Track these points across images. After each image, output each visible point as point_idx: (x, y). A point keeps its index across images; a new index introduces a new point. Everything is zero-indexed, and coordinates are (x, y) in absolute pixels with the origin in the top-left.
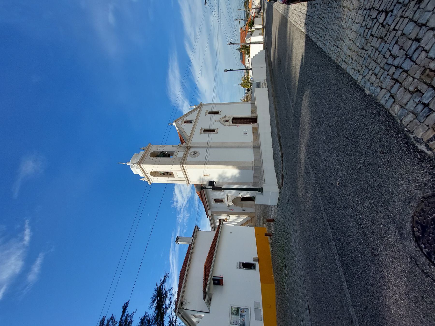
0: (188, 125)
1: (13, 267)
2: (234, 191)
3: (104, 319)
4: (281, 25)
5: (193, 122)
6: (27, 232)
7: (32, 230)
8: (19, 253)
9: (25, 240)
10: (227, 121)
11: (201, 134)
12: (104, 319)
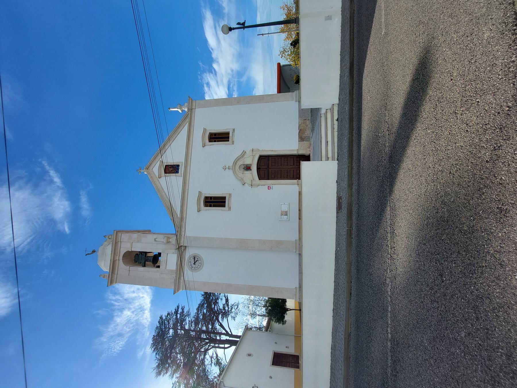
0: (172, 177)
1: (62, 207)
2: (258, 22)
3: (178, 307)
4: (408, 98)
5: (182, 169)
6: (52, 173)
7: (57, 171)
8: (59, 194)
9: (56, 182)
10: (248, 168)
11: (204, 146)
12: (178, 307)
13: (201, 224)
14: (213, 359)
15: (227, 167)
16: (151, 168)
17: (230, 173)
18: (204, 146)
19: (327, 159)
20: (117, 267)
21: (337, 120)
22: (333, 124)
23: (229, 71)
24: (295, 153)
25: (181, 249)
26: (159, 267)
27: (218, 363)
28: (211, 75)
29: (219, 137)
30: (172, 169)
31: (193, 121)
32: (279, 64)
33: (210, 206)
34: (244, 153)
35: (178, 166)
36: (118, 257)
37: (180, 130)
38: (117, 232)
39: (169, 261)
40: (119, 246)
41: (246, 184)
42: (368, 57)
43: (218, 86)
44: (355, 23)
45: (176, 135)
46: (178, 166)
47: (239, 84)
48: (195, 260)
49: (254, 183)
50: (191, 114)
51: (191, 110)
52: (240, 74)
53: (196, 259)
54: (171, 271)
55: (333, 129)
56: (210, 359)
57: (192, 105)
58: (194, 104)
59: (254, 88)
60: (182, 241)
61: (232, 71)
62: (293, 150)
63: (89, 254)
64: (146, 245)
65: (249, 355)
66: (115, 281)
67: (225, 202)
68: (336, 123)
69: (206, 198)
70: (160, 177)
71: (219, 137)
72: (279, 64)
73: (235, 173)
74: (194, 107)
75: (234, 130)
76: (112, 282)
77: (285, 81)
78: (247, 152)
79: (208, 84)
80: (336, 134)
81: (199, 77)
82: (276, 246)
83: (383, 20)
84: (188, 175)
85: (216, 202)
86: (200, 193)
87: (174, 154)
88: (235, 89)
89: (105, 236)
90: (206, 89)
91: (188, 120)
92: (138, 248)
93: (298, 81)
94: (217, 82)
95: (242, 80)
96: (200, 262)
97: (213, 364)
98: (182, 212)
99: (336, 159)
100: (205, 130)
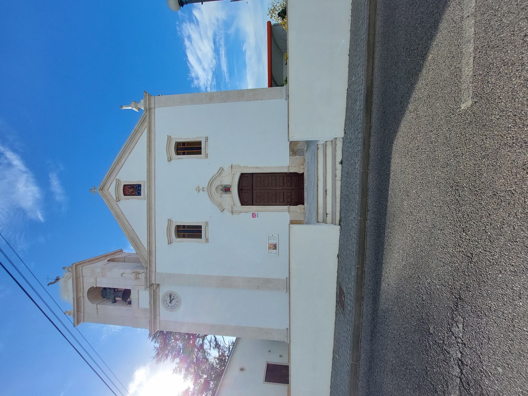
0: (132, 201)
5: (144, 190)
10: (227, 189)
11: (170, 160)
13: (174, 257)
14: (211, 343)
15: (201, 188)
16: (106, 188)
17: (204, 195)
18: (170, 160)
19: (325, 222)
20: (82, 305)
21: (341, 163)
22: (334, 169)
23: (214, 21)
24: (285, 171)
25: (153, 287)
26: (130, 303)
27: (217, 346)
28: (193, 26)
29: (189, 148)
30: (132, 190)
31: (153, 126)
32: (269, 23)
33: (184, 237)
34: (221, 170)
35: (140, 186)
36: (81, 293)
37: (137, 137)
38: (76, 266)
39: (141, 297)
40: (82, 280)
41: (225, 211)
42: (408, 117)
43: (202, 40)
44: (378, 12)
45: (133, 144)
46: (140, 186)
47: (227, 37)
48: (171, 297)
49: (235, 209)
50: (150, 116)
51: (149, 110)
52: (227, 24)
53: (172, 297)
54: (145, 310)
55: (334, 176)
56: (208, 344)
57: (149, 104)
58: (152, 101)
59: (244, 42)
60: (153, 279)
61: (218, 20)
62: (283, 167)
63: (51, 283)
64: (114, 277)
65: (242, 370)
66: (82, 319)
67: (201, 232)
68: (339, 167)
69: (178, 227)
70: (118, 200)
71: (189, 148)
72: (269, 23)
73: (211, 196)
74: (153, 106)
75: (207, 139)
76: (78, 322)
77: (277, 45)
78: (225, 169)
79: (189, 37)
80: (338, 184)
81: (178, 28)
82: (265, 284)
83: (468, 71)
84: (153, 197)
85: (190, 232)
86: (170, 221)
87: (132, 170)
88: (222, 43)
89: (64, 268)
90: (187, 43)
91: (146, 124)
92: (104, 283)
93: (286, 81)
94: (200, 35)
95: (230, 32)
96: (176, 300)
97: (212, 348)
98: (149, 243)
99: (337, 222)
100: (169, 138)
